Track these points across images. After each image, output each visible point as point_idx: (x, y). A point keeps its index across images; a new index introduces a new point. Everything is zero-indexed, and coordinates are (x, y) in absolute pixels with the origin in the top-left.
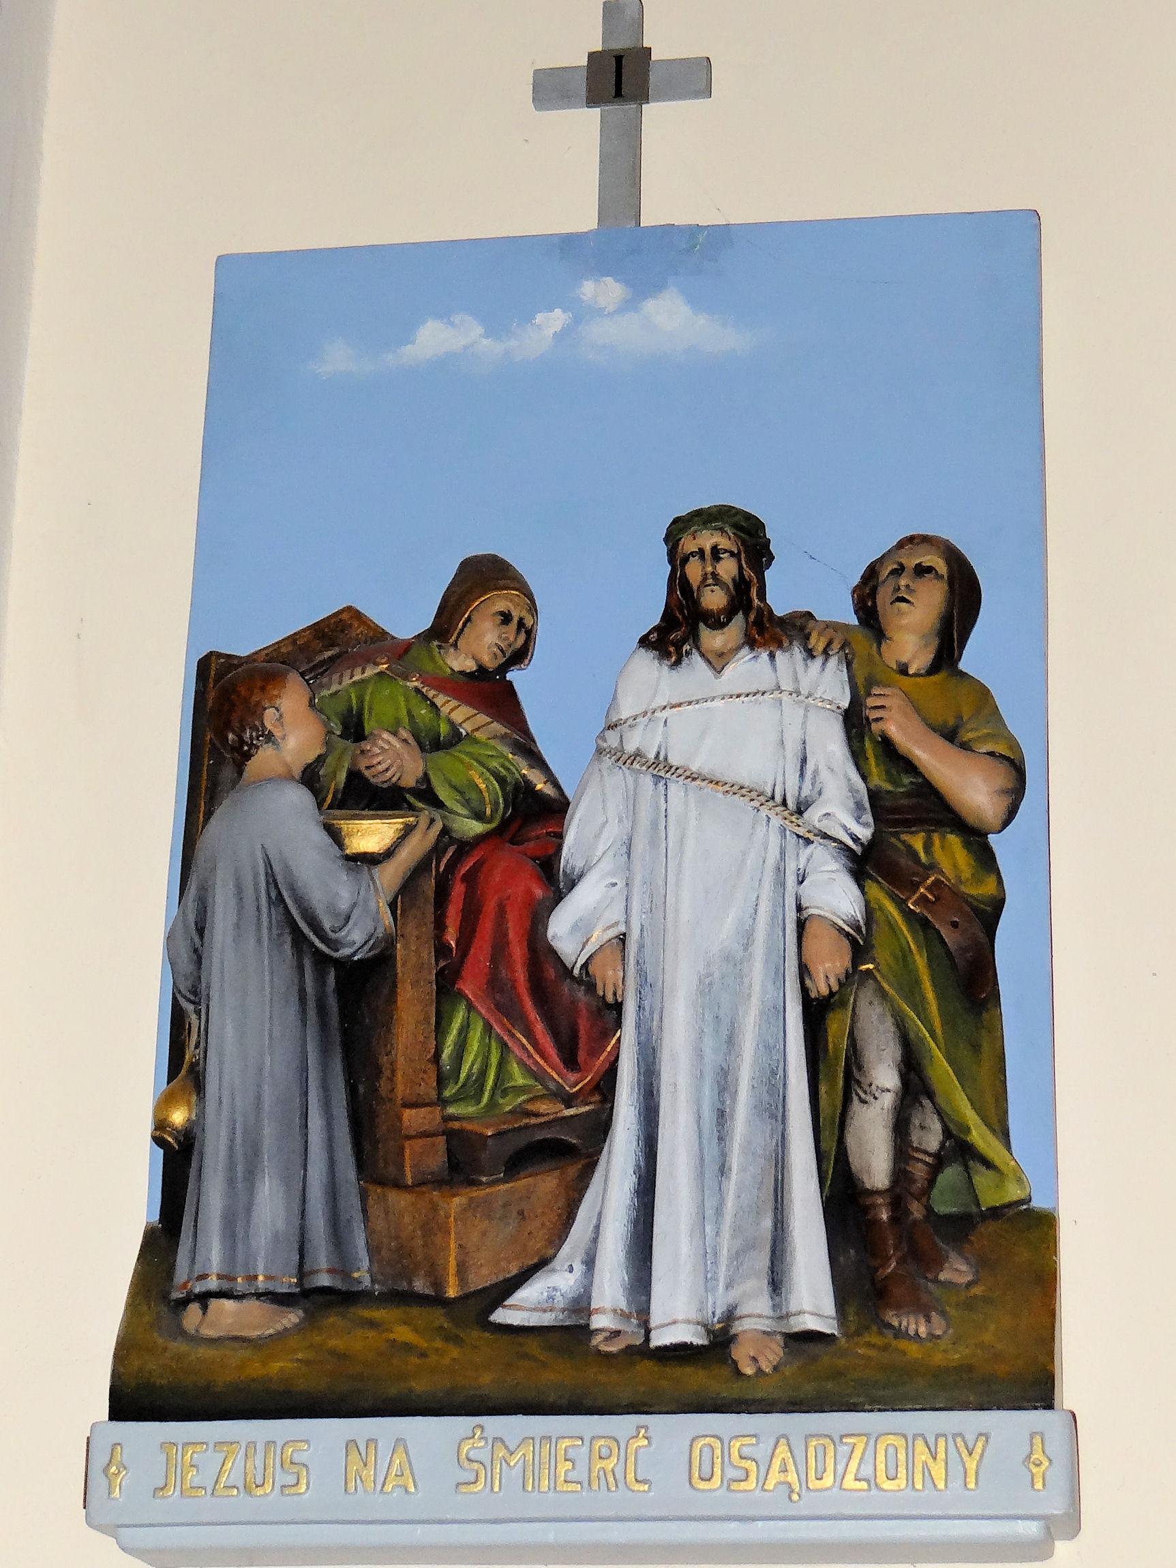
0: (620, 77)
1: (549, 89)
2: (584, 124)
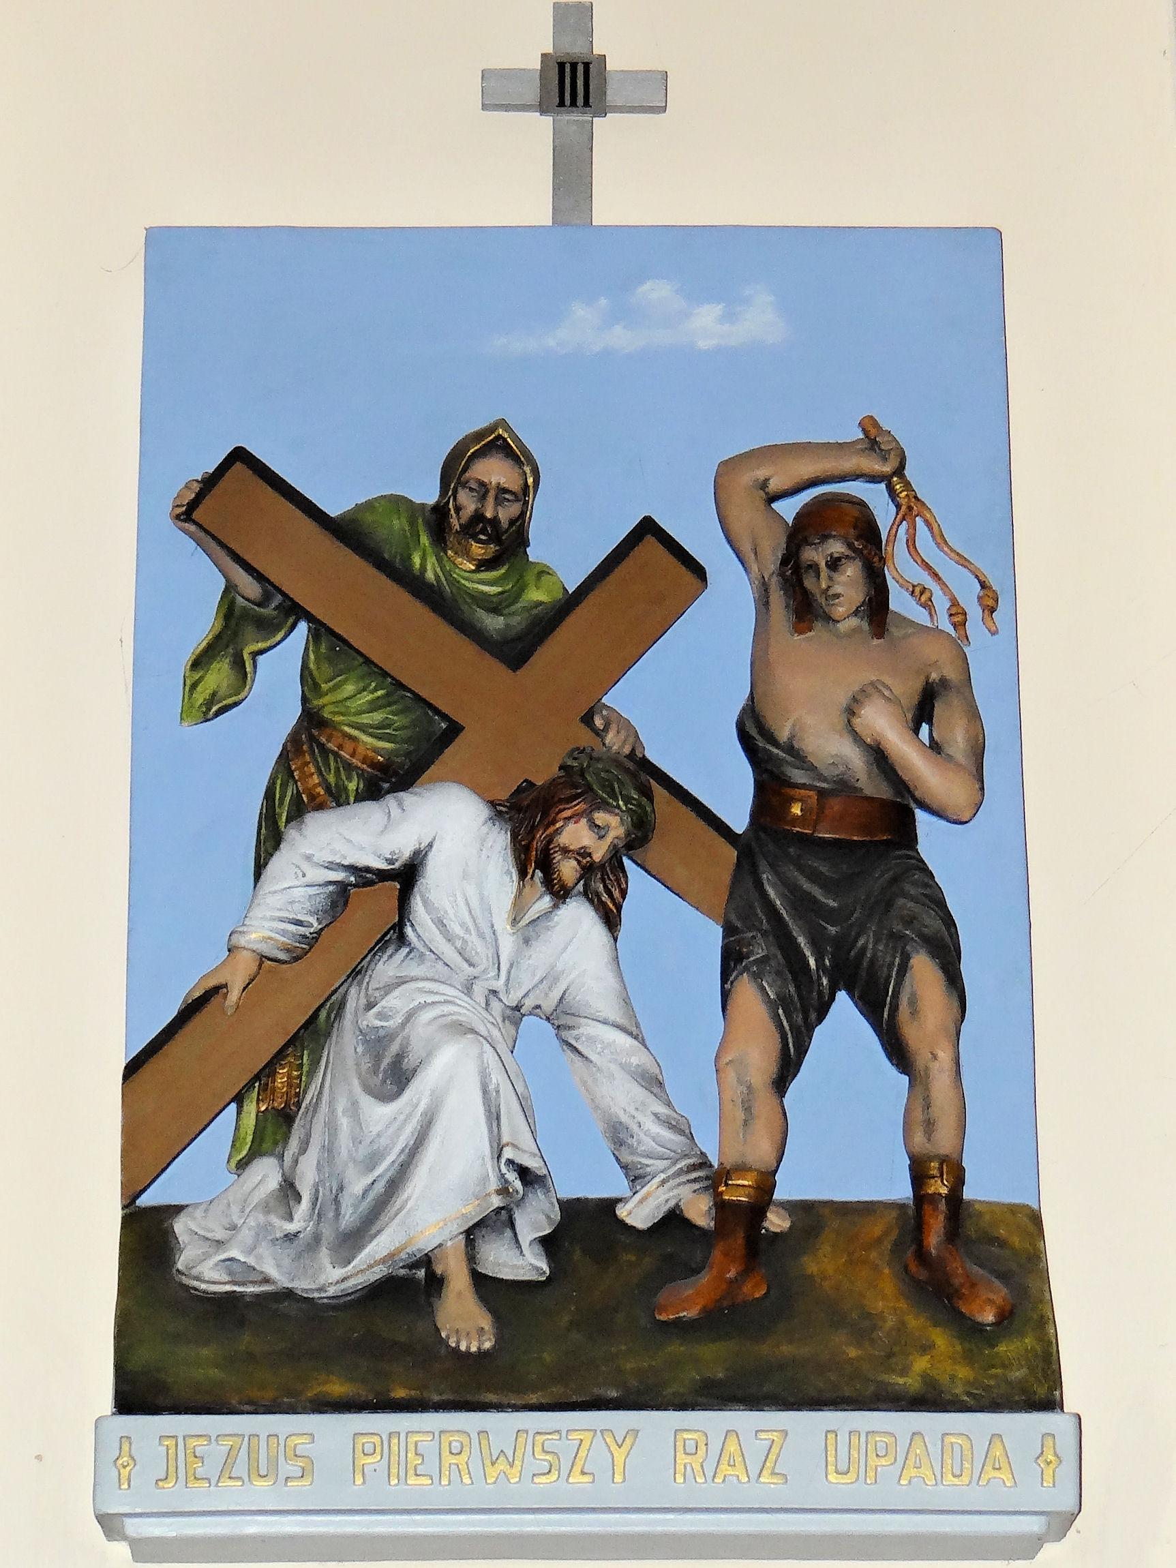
0: (573, 84)
2: (538, 131)
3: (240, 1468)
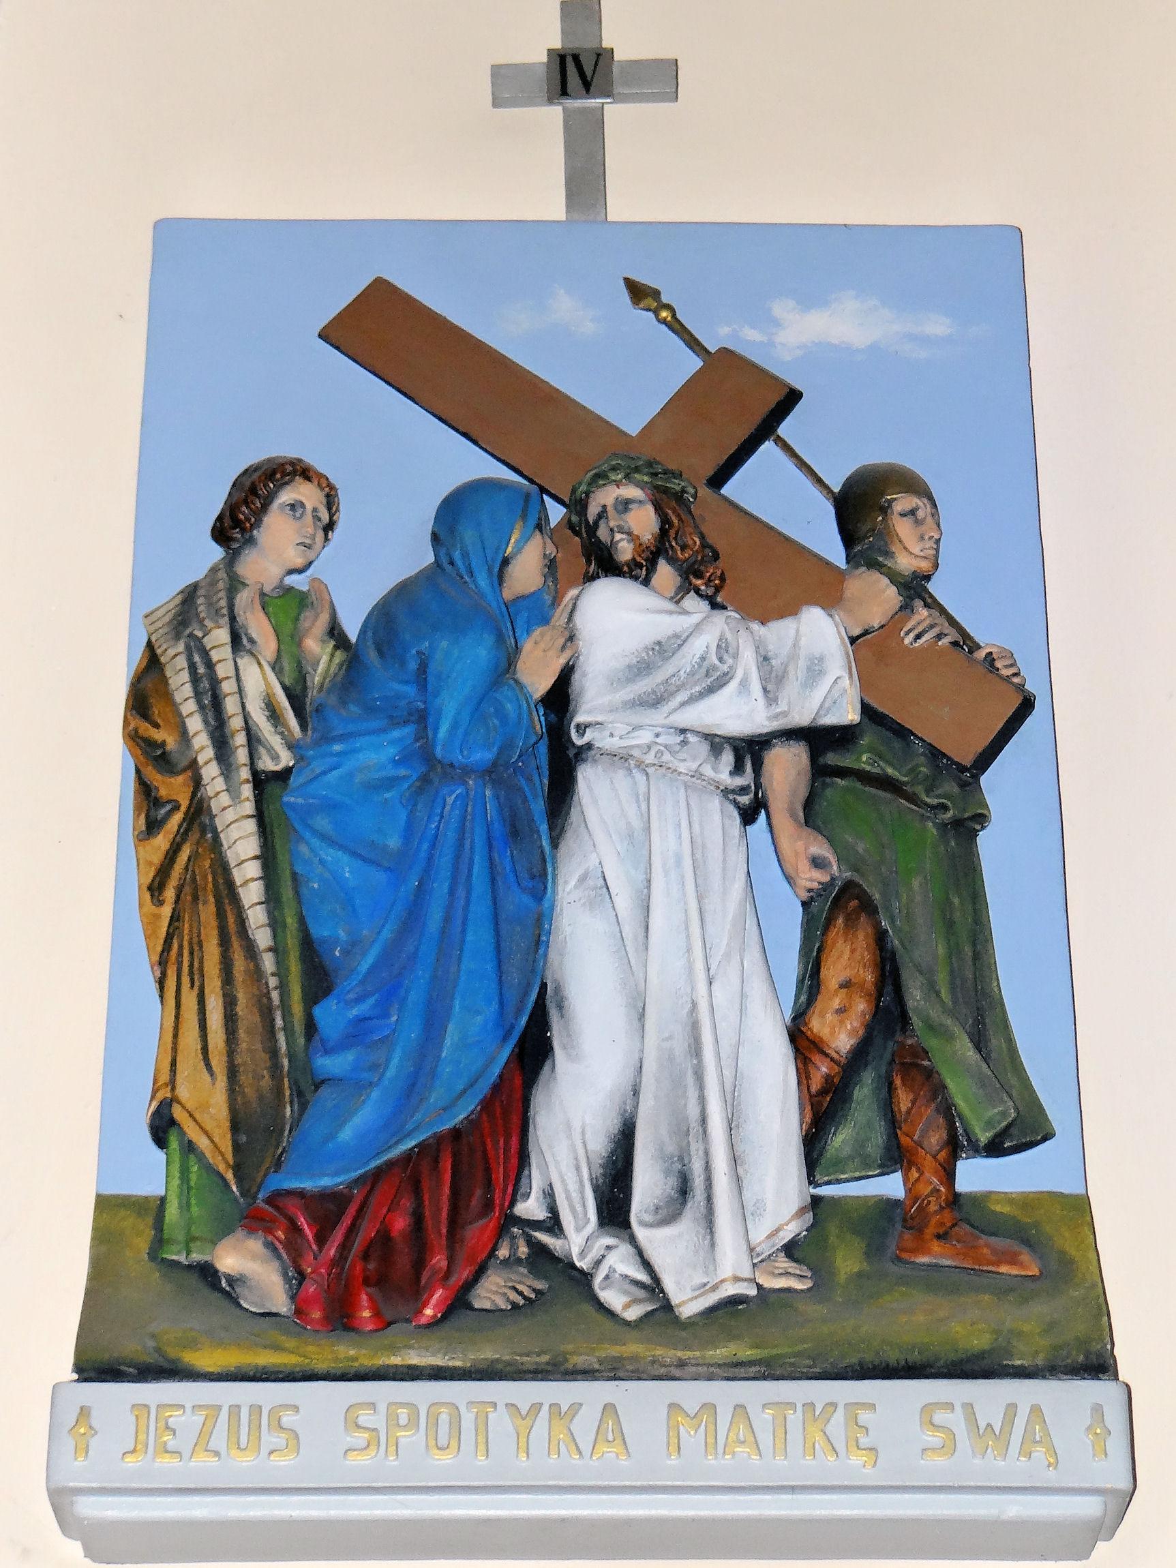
0: (578, 72)
1: (507, 85)
3: (219, 1440)
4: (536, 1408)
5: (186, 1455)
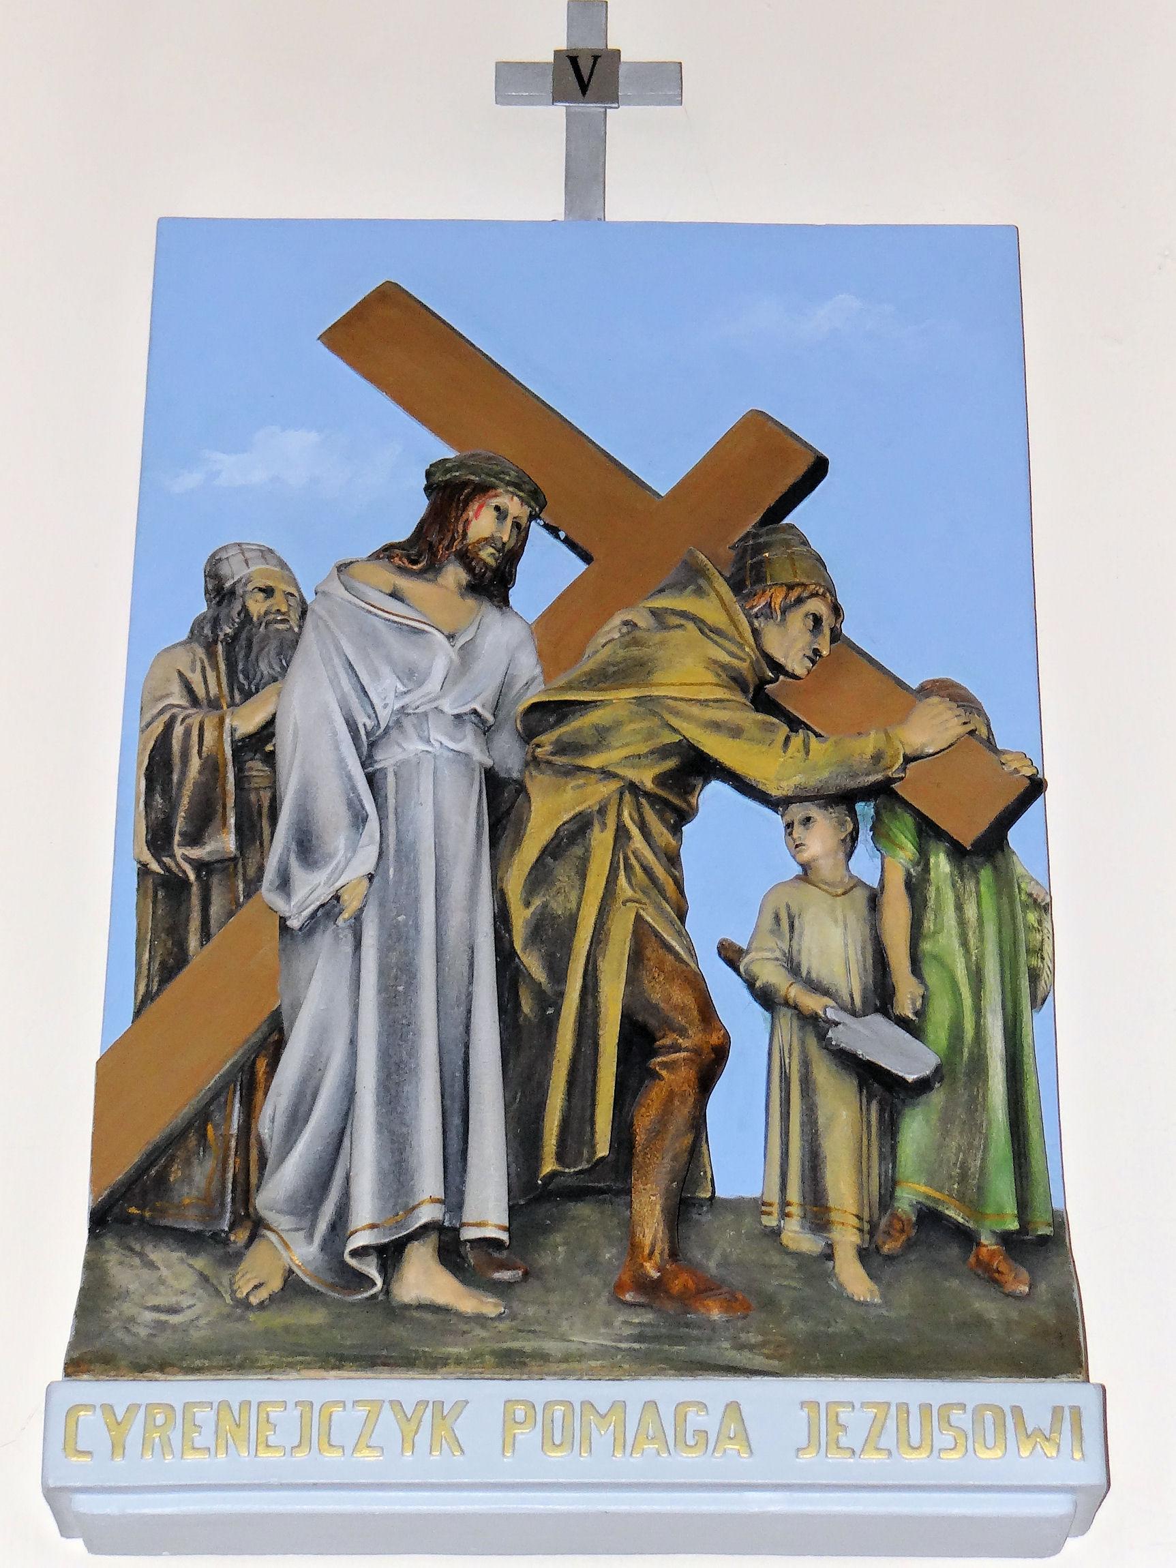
0: (585, 75)
1: (512, 80)
2: (551, 119)
3: (888, 1440)
4: (132, 1408)
5: (348, 1451)
